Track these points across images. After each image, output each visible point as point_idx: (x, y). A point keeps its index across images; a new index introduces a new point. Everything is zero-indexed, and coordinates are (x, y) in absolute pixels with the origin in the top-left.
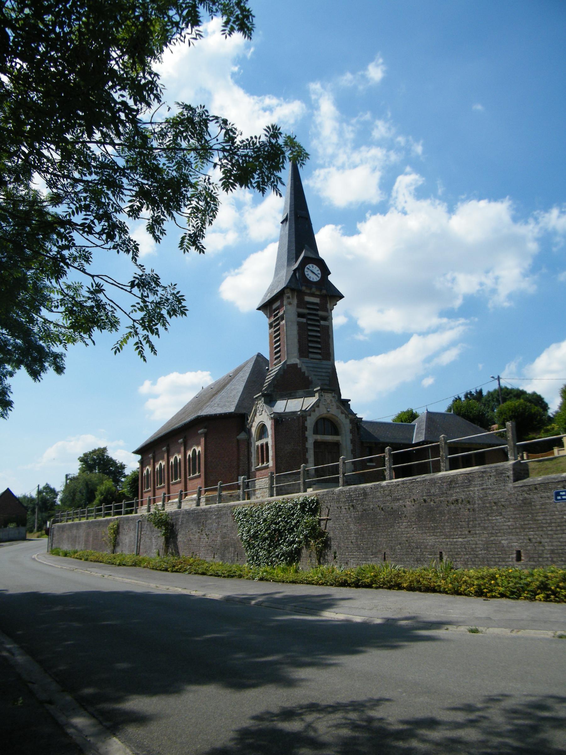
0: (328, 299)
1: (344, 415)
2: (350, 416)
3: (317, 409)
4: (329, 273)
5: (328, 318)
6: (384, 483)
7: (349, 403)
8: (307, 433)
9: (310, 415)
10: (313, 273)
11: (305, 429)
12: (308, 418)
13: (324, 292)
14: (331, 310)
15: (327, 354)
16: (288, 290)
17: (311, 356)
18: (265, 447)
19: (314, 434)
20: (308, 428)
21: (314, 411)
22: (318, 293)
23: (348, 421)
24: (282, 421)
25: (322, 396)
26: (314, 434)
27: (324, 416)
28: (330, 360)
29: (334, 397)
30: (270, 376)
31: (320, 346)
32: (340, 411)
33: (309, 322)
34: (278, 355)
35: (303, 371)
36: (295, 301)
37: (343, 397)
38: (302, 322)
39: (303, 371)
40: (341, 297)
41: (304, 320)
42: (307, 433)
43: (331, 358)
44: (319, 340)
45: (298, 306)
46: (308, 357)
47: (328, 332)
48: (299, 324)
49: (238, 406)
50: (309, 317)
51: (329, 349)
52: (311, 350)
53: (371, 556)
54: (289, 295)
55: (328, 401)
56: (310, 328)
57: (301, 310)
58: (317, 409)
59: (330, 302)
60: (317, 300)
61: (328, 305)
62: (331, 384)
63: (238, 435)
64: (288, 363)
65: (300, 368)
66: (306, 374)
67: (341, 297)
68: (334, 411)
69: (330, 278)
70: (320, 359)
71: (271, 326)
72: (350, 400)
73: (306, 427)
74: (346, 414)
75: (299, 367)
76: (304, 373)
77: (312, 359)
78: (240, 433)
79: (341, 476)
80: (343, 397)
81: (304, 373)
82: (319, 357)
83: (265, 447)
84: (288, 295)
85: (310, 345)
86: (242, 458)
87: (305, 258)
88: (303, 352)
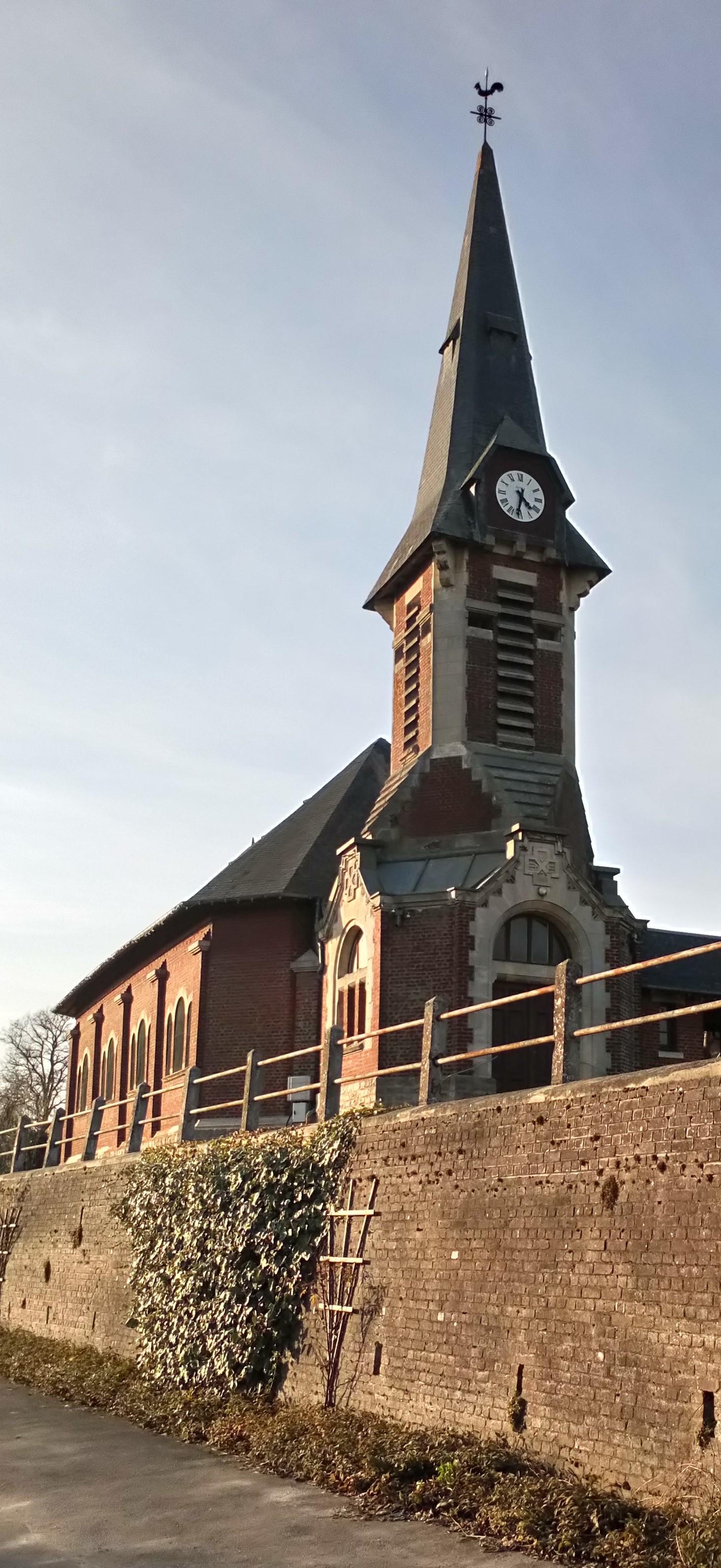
0: (563, 575)
1: (588, 909)
2: (607, 912)
3: (506, 887)
4: (570, 501)
5: (559, 632)
6: (538, 1096)
7: (615, 878)
8: (474, 956)
9: (485, 904)
10: (516, 492)
11: (469, 943)
12: (479, 912)
13: (552, 553)
14: (572, 610)
15: (551, 730)
16: (442, 544)
17: (502, 735)
18: (357, 992)
19: (496, 958)
20: (477, 942)
21: (499, 892)
22: (532, 557)
23: (600, 925)
24: (403, 917)
25: (524, 849)
26: (496, 958)
27: (528, 908)
28: (559, 752)
29: (559, 854)
30: (387, 792)
31: (530, 710)
32: (576, 895)
33: (501, 641)
34: (411, 735)
35: (474, 778)
36: (463, 578)
37: (597, 862)
38: (481, 641)
39: (474, 778)
40: (603, 571)
41: (488, 634)
42: (473, 955)
43: (564, 747)
44: (530, 693)
45: (472, 593)
46: (494, 740)
47: (558, 672)
48: (472, 645)
49: (295, 882)
50: (502, 625)
51: (559, 721)
52: (502, 720)
53: (480, 1374)
54: (448, 558)
55: (543, 866)
56: (502, 656)
57: (479, 605)
58: (506, 887)
59: (568, 585)
60: (528, 579)
61: (563, 594)
62: (561, 818)
63: (294, 959)
64: (435, 756)
65: (468, 771)
66: (485, 789)
67: (603, 571)
68: (560, 895)
69: (570, 514)
70: (528, 748)
71: (398, 654)
72: (617, 871)
73: (473, 938)
74: (594, 907)
75: (465, 766)
76: (478, 784)
77: (504, 744)
78: (301, 953)
79: (424, 1065)
80: (597, 862)
81: (478, 784)
82: (529, 740)
83: (357, 992)
84: (441, 557)
85: (501, 705)
86: (300, 1024)
87: (498, 447)
88: (480, 723)
